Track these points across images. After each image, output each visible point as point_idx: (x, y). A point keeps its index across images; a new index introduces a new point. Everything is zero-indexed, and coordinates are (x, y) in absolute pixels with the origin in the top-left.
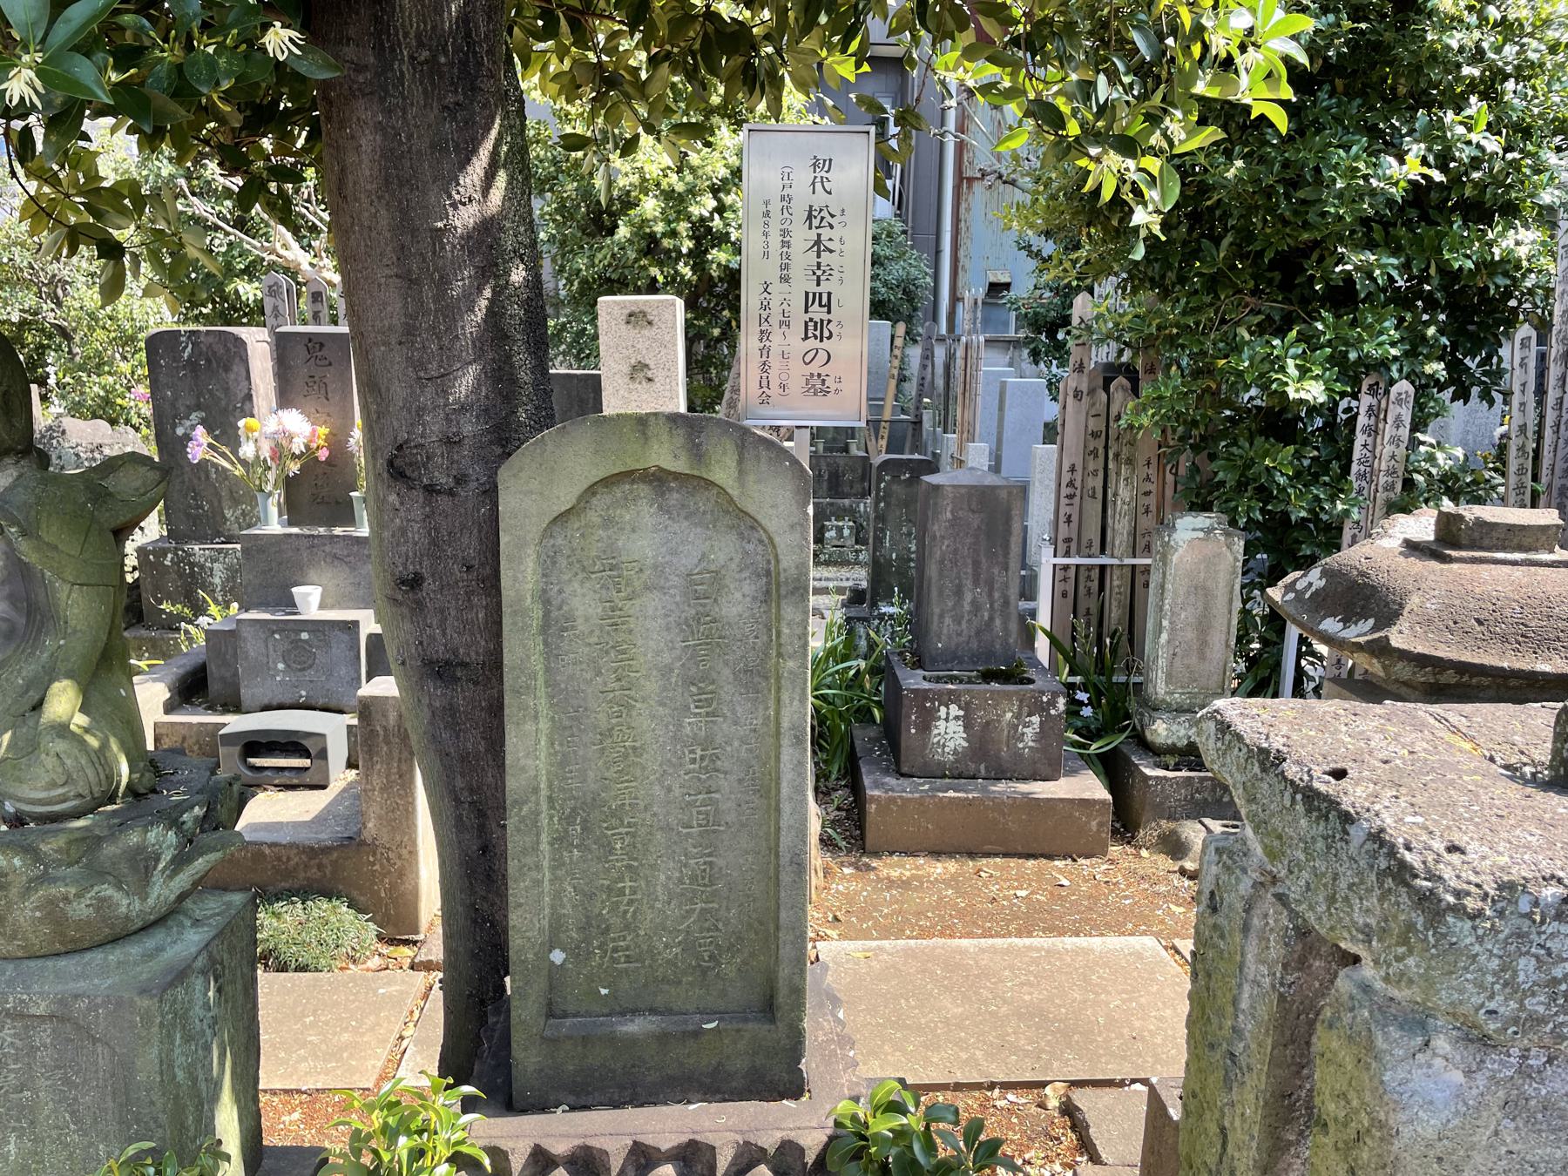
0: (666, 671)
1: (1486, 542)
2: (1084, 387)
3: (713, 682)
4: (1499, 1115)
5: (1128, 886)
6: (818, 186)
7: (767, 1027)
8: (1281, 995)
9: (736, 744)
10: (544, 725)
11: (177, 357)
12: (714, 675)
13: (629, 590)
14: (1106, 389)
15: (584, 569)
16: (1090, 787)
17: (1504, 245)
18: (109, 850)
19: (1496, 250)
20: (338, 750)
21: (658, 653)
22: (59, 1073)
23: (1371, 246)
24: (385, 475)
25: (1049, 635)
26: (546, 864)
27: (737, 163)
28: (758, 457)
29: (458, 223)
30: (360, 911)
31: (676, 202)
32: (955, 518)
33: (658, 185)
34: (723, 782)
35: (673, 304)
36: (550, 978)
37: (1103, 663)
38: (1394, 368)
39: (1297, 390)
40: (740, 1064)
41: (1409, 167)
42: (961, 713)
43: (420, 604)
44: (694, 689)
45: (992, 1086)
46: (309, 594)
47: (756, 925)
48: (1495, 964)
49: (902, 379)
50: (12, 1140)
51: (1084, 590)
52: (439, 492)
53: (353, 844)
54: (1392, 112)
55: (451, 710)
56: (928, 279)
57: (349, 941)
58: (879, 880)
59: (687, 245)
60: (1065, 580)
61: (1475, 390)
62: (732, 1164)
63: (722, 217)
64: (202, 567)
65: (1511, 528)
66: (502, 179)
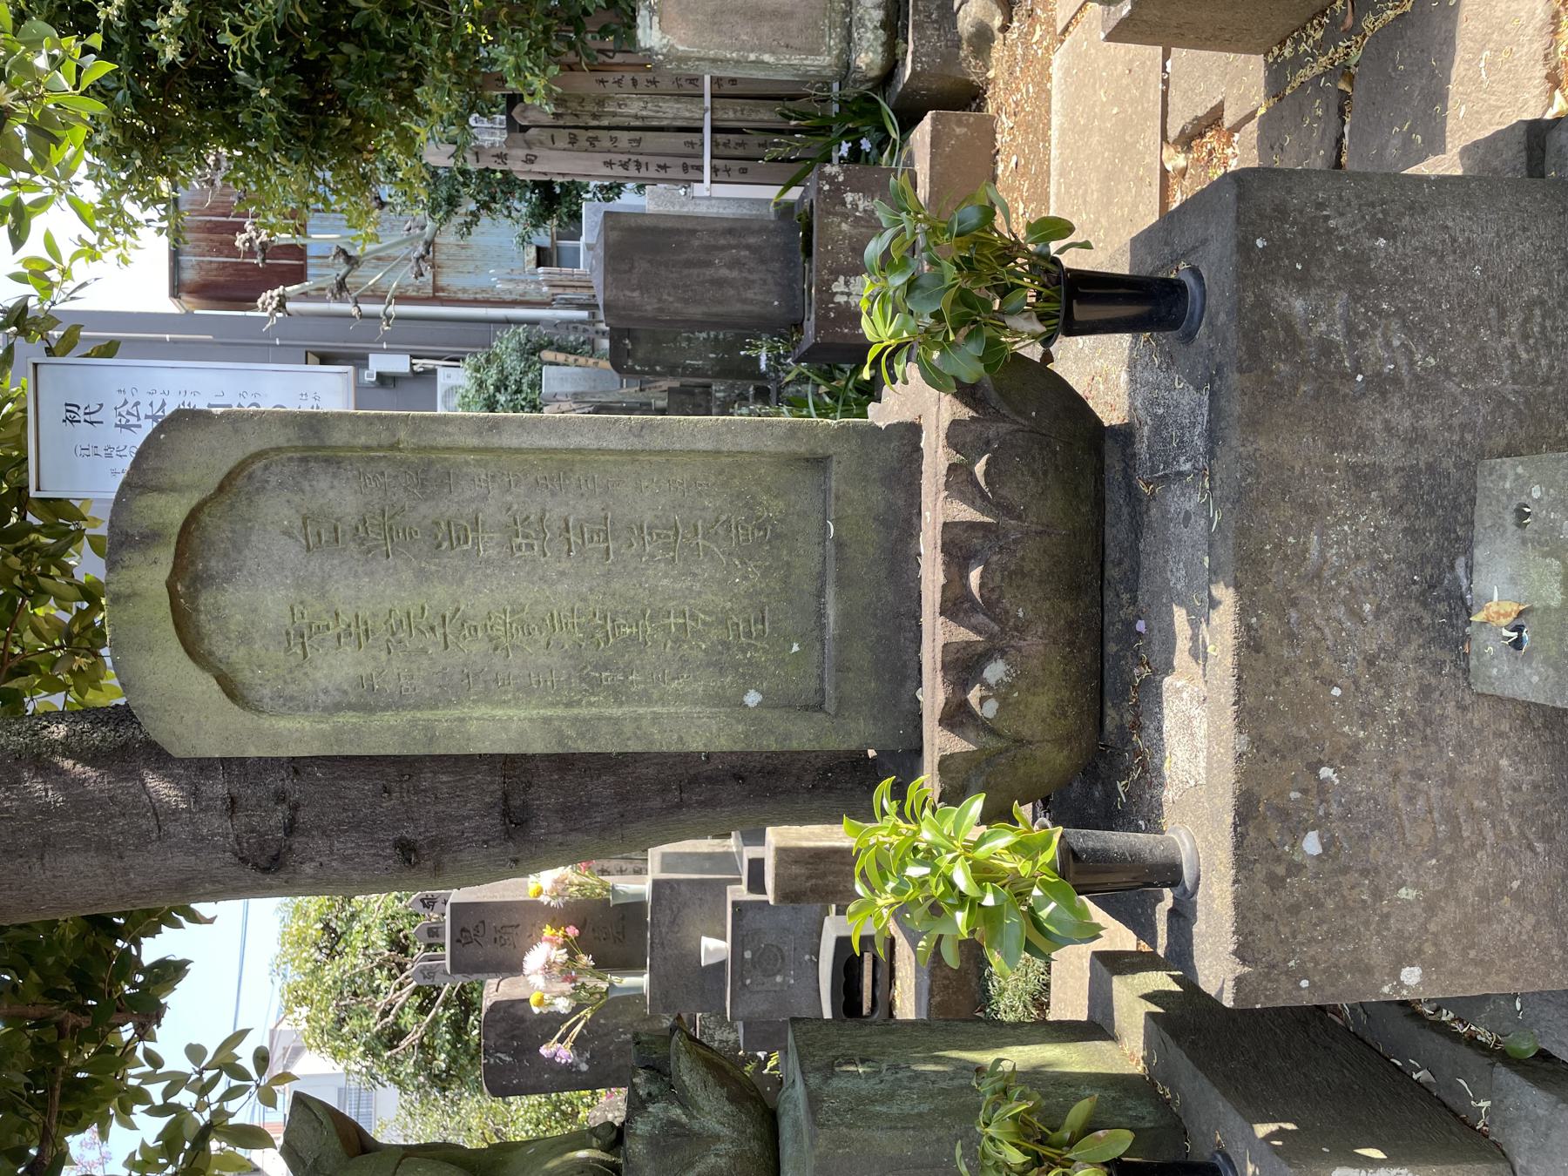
0: (421, 575)
2: (521, 153)
3: (437, 524)
5: (1018, 90)
6: (93, 418)
7: (834, 464)
9: (509, 498)
13: (325, 616)
14: (524, 129)
25: (787, 187)
28: (156, 470)
32: (639, 287)
34: (555, 514)
37: (819, 128)
40: (877, 496)
42: (842, 279)
43: (432, 844)
44: (445, 544)
46: (707, 949)
47: (723, 478)
51: (738, 153)
52: (293, 820)
60: (728, 171)
62: (972, 504)
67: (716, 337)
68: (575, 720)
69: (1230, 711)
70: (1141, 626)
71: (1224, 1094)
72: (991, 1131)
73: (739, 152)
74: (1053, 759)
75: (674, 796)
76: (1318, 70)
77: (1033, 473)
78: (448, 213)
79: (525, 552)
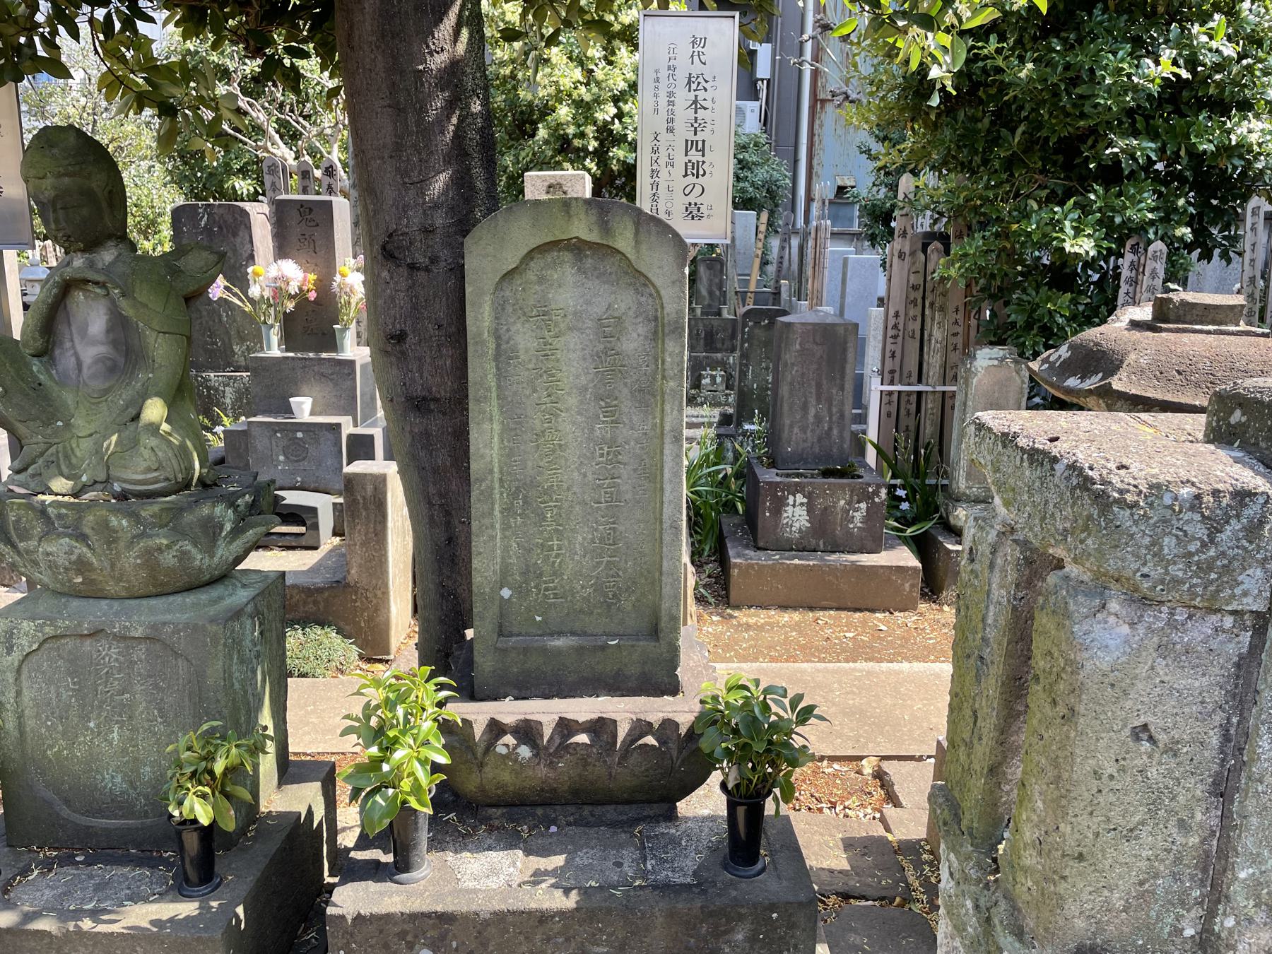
1: (1188, 318)
2: (907, 249)
4: (1155, 655)
5: (932, 631)
6: (696, 58)
8: (1014, 606)
10: (496, 427)
11: (196, 225)
12: (617, 392)
14: (924, 251)
15: (524, 314)
16: (905, 558)
17: (1239, 132)
18: (188, 518)
19: (1233, 137)
20: (326, 521)
21: (577, 377)
22: (151, 681)
23: (1135, 134)
24: (380, 257)
26: (498, 526)
27: (634, 78)
28: (649, 232)
29: (433, 67)
30: (345, 636)
31: (584, 109)
32: (803, 349)
33: (570, 95)
35: (583, 178)
36: (501, 607)
38: (1151, 231)
39: (1072, 246)
40: (634, 670)
41: (1163, 67)
42: (805, 500)
43: (403, 353)
44: (602, 403)
45: (822, 759)
46: (302, 403)
48: (1147, 541)
49: (764, 263)
50: (116, 730)
51: (902, 411)
52: (418, 269)
53: (340, 586)
54: (1152, 25)
55: (426, 434)
56: (787, 181)
57: (337, 657)
58: (740, 625)
59: (593, 145)
60: (889, 403)
61: (1217, 252)
62: (628, 735)
63: (621, 122)
64: (216, 390)
65: (1207, 307)
66: (465, 33)
67: (768, 389)
68: (492, 489)
69: (503, 907)
70: (553, 829)
71: (258, 880)
72: (234, 750)
73: (903, 411)
74: (471, 783)
75: (436, 500)
76: (911, 879)
77: (647, 770)
78: (876, 136)
79: (598, 452)
